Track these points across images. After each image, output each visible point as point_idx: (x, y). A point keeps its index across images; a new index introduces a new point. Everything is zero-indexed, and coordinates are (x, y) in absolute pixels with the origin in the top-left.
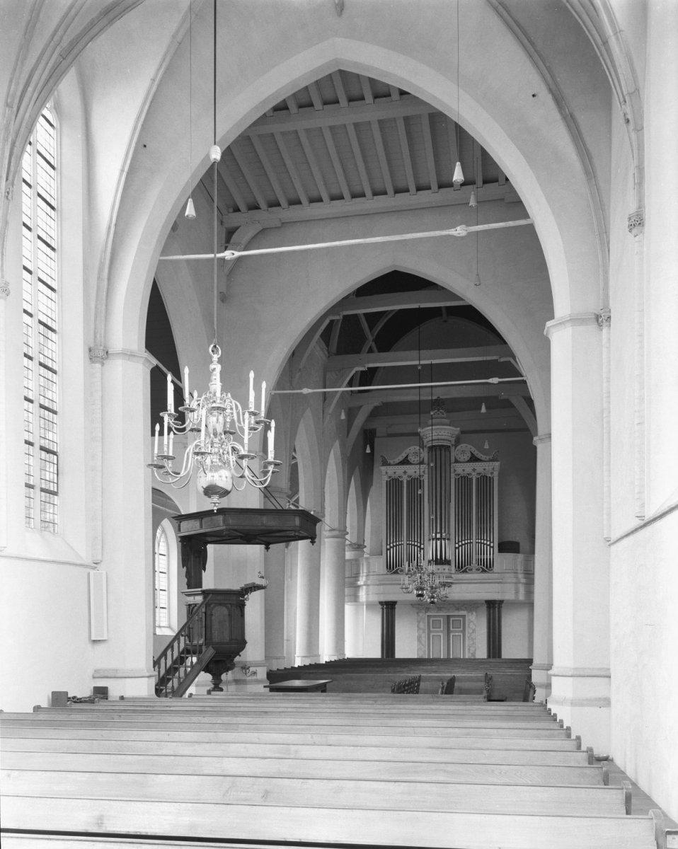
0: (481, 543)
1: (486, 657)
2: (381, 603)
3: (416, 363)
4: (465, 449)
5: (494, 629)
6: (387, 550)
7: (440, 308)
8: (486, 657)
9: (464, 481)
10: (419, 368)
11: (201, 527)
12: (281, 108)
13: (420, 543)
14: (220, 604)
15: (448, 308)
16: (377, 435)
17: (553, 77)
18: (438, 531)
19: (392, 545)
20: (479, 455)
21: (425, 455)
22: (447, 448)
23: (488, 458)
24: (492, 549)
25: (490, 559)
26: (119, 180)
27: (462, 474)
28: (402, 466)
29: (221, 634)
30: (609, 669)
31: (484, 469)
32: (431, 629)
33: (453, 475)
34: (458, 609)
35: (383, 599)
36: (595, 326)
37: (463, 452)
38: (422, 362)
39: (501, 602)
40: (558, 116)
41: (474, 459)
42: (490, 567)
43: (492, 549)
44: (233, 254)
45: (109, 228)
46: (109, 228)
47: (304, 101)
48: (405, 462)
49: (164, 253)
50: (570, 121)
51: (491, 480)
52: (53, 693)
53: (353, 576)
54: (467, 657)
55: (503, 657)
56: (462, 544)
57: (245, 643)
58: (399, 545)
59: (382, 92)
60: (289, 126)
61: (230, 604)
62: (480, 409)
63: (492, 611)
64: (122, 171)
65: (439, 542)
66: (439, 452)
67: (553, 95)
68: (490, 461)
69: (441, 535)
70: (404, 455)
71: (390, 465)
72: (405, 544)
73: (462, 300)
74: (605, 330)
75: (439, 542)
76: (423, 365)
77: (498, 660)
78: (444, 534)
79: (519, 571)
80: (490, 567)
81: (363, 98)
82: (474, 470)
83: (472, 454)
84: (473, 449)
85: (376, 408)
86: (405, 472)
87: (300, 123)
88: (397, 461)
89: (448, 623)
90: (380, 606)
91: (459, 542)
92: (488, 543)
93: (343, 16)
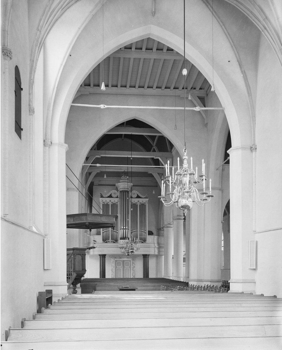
0: (114, 231)
1: (143, 277)
2: (100, 255)
3: (130, 156)
4: (135, 193)
5: (146, 266)
6: (103, 233)
7: (122, 135)
8: (143, 277)
9: (134, 206)
10: (131, 159)
11: (74, 221)
12: (128, 48)
13: (117, 230)
14: (78, 254)
15: (125, 135)
16: (94, 184)
17: (239, 56)
18: (124, 226)
19: (105, 231)
20: (140, 195)
21: (118, 194)
22: (128, 192)
23: (144, 197)
24: (145, 234)
25: (145, 238)
26: (60, 69)
27: (114, 202)
28: (109, 198)
29: (78, 268)
30: (254, 280)
31: (134, 201)
32: (117, 266)
33: (130, 203)
34: (120, 258)
35: (101, 253)
36: (249, 151)
37: (134, 194)
38: (133, 156)
39: (149, 255)
40: (240, 71)
41: (138, 197)
42: (117, 241)
43: (145, 234)
44: (104, 106)
45: (54, 89)
46: (54, 89)
47: (139, 46)
48: (110, 196)
49: (73, 102)
50: (244, 72)
51: (117, 206)
52: (52, 290)
53: (87, 243)
54: (131, 277)
55: (106, 277)
56: (107, 231)
57: (86, 271)
58: (108, 231)
59: (160, 48)
60: (127, 56)
61: (82, 254)
62: (104, 176)
63: (145, 259)
64: (62, 65)
65: (125, 230)
66: (125, 193)
67: (238, 62)
68: (145, 198)
69: (126, 227)
70: (110, 194)
71: (104, 197)
72: (138, 231)
73: (160, 133)
74: (254, 153)
75: (125, 230)
76: (133, 158)
77: (104, 279)
78: (127, 227)
79: (155, 243)
80: (117, 241)
81: (141, 49)
82: (110, 201)
83: (138, 195)
84: (138, 193)
85: (98, 173)
86: (138, 201)
87: (134, 55)
88: (107, 196)
89: (124, 263)
90: (99, 256)
91: (132, 230)
92: (144, 231)
93: (155, 16)
